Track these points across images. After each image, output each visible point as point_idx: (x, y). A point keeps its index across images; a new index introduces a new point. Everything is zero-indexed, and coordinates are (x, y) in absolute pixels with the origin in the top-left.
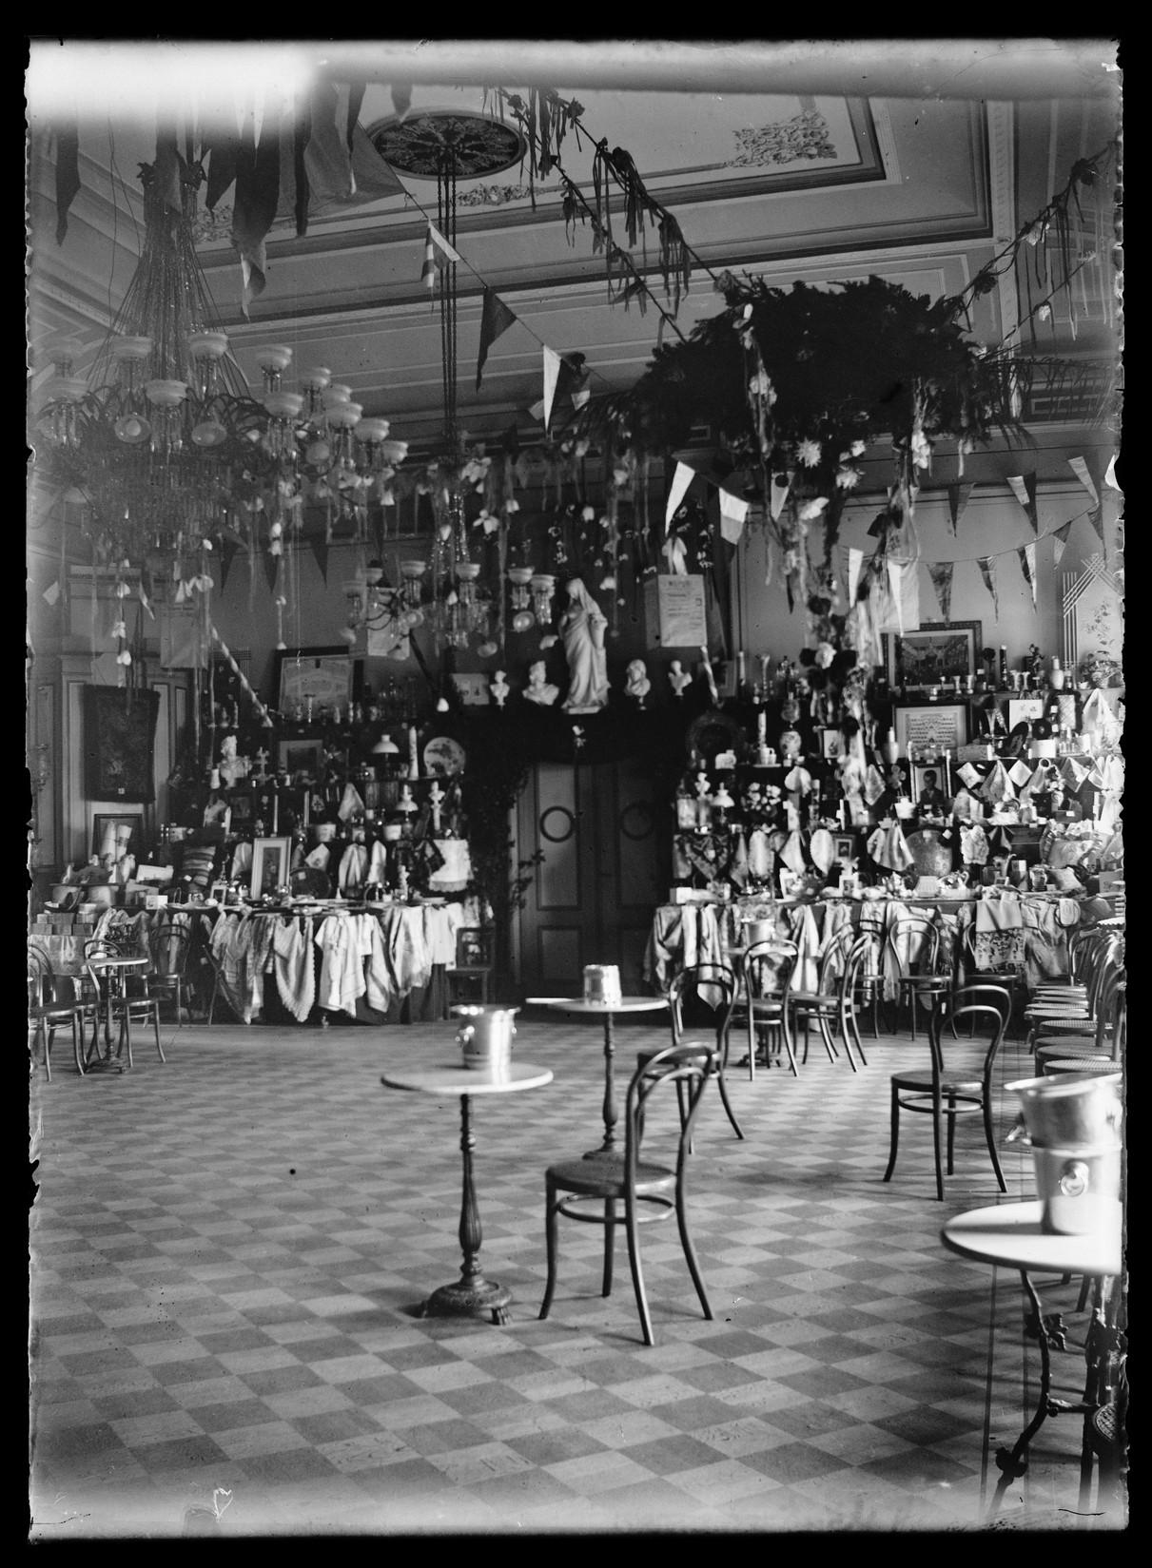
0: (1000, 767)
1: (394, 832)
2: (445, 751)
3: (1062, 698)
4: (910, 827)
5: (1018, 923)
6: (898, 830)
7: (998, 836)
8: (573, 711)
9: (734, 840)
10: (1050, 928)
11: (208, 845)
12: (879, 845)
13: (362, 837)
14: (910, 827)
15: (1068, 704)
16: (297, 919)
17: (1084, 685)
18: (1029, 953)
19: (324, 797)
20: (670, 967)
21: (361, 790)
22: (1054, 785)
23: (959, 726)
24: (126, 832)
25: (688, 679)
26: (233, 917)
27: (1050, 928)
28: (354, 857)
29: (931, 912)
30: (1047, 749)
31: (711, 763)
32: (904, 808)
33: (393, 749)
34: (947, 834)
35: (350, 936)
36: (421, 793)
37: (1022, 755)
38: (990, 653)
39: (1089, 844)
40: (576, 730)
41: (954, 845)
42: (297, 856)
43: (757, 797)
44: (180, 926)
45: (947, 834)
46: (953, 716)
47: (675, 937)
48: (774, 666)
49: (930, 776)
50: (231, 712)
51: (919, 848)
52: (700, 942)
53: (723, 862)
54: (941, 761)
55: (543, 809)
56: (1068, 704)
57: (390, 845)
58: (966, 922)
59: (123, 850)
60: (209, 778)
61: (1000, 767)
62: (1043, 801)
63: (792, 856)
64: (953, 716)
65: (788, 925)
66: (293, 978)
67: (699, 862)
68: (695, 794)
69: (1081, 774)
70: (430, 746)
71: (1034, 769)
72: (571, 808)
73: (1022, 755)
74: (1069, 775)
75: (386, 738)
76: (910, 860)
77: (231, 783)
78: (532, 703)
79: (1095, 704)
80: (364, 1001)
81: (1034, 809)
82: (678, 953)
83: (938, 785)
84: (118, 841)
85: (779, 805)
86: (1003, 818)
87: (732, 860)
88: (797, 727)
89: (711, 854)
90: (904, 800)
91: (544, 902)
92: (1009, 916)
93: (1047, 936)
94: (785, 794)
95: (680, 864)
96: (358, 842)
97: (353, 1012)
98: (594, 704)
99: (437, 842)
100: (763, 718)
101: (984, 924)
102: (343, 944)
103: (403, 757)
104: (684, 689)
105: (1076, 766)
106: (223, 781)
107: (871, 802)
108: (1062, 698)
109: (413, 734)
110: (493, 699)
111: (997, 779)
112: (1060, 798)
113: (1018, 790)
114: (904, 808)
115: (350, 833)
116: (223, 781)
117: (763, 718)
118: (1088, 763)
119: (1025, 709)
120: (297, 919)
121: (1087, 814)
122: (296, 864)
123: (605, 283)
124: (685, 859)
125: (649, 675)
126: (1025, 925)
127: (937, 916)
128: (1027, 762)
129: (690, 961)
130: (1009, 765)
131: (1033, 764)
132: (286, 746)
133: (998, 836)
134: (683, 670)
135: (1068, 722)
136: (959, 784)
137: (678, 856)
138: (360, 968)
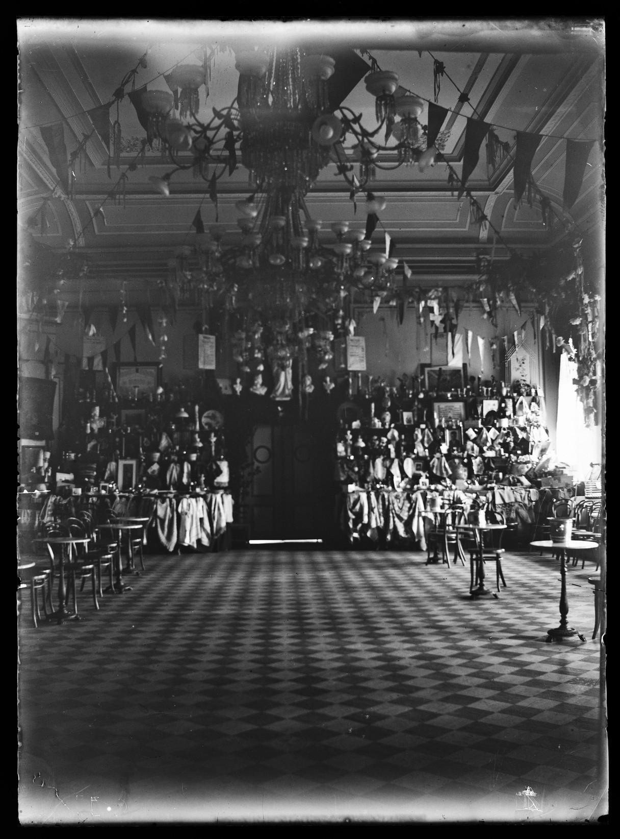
0: (485, 430)
1: (194, 457)
2: (213, 417)
3: (507, 400)
4: (449, 457)
5: (513, 500)
6: (444, 459)
7: (489, 461)
8: (278, 399)
9: (367, 462)
10: (526, 502)
11: (93, 463)
12: (436, 464)
13: (176, 459)
14: (449, 457)
15: (510, 403)
16: (168, 500)
17: (515, 395)
18: (517, 513)
19: (150, 439)
20: (355, 523)
21: (170, 435)
22: (509, 439)
23: (462, 412)
24: (48, 455)
25: (333, 386)
26: (124, 499)
27: (526, 502)
28: (173, 471)
29: (474, 495)
30: (505, 423)
31: (350, 426)
32: (444, 448)
33: (186, 415)
34: (466, 461)
35: (194, 508)
36: (205, 438)
37: (494, 425)
38: (473, 378)
39: (530, 466)
40: (279, 408)
41: (469, 466)
42: (142, 468)
43: (377, 442)
44: (93, 503)
45: (466, 461)
46: (459, 407)
47: (358, 507)
48: (375, 381)
49: (453, 435)
50: (91, 394)
51: (454, 468)
52: (371, 509)
53: (362, 473)
54: (458, 427)
55: (255, 447)
56: (510, 403)
57: (192, 463)
58: (490, 500)
59: (46, 465)
60: (85, 427)
61: (485, 430)
62: (505, 445)
63: (395, 470)
64: (459, 407)
65: (410, 502)
66: (166, 529)
67: (350, 473)
68: (346, 441)
69: (522, 435)
70: (205, 414)
71: (499, 431)
72: (269, 446)
73: (494, 425)
74: (515, 435)
75: (183, 410)
76: (450, 472)
77: (96, 431)
78: (256, 394)
79: (521, 403)
80: (199, 541)
81: (502, 450)
82: (359, 515)
83: (457, 438)
84: (45, 460)
85: (387, 446)
86: (490, 454)
87: (367, 473)
88: (390, 410)
89: (356, 469)
90: (443, 445)
91: (255, 493)
92: (509, 497)
93: (525, 505)
94: (389, 442)
95: (341, 474)
96: (174, 461)
97: (195, 546)
98: (287, 396)
99: (218, 463)
100: (373, 405)
101: (498, 501)
102: (191, 512)
103: (192, 420)
104: (331, 390)
105: (518, 431)
106: (92, 429)
107: (426, 445)
108: (507, 400)
109: (197, 408)
110: (234, 391)
111: (484, 436)
112: (512, 444)
113: (493, 441)
114: (444, 448)
115: (169, 457)
116: (92, 429)
117: (373, 405)
118: (523, 429)
119: (490, 405)
120: (168, 500)
121: (526, 452)
122: (141, 473)
123: (449, 193)
124: (344, 472)
125: (313, 383)
126: (516, 501)
127: (477, 497)
128: (496, 429)
129: (366, 520)
130: (488, 430)
131: (499, 429)
132: (124, 412)
133: (489, 461)
134: (331, 381)
135: (509, 412)
136: (467, 438)
137: (340, 470)
138: (199, 523)
